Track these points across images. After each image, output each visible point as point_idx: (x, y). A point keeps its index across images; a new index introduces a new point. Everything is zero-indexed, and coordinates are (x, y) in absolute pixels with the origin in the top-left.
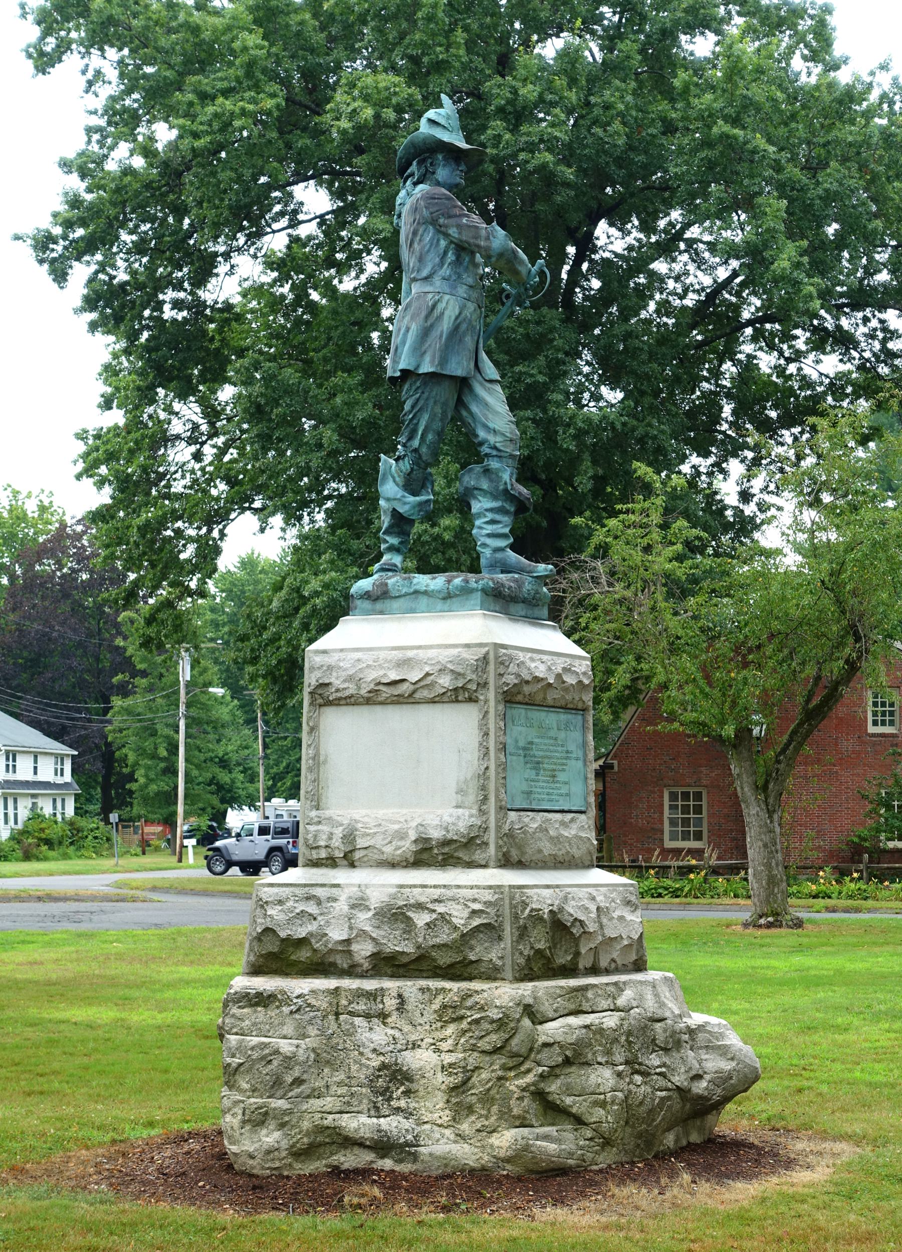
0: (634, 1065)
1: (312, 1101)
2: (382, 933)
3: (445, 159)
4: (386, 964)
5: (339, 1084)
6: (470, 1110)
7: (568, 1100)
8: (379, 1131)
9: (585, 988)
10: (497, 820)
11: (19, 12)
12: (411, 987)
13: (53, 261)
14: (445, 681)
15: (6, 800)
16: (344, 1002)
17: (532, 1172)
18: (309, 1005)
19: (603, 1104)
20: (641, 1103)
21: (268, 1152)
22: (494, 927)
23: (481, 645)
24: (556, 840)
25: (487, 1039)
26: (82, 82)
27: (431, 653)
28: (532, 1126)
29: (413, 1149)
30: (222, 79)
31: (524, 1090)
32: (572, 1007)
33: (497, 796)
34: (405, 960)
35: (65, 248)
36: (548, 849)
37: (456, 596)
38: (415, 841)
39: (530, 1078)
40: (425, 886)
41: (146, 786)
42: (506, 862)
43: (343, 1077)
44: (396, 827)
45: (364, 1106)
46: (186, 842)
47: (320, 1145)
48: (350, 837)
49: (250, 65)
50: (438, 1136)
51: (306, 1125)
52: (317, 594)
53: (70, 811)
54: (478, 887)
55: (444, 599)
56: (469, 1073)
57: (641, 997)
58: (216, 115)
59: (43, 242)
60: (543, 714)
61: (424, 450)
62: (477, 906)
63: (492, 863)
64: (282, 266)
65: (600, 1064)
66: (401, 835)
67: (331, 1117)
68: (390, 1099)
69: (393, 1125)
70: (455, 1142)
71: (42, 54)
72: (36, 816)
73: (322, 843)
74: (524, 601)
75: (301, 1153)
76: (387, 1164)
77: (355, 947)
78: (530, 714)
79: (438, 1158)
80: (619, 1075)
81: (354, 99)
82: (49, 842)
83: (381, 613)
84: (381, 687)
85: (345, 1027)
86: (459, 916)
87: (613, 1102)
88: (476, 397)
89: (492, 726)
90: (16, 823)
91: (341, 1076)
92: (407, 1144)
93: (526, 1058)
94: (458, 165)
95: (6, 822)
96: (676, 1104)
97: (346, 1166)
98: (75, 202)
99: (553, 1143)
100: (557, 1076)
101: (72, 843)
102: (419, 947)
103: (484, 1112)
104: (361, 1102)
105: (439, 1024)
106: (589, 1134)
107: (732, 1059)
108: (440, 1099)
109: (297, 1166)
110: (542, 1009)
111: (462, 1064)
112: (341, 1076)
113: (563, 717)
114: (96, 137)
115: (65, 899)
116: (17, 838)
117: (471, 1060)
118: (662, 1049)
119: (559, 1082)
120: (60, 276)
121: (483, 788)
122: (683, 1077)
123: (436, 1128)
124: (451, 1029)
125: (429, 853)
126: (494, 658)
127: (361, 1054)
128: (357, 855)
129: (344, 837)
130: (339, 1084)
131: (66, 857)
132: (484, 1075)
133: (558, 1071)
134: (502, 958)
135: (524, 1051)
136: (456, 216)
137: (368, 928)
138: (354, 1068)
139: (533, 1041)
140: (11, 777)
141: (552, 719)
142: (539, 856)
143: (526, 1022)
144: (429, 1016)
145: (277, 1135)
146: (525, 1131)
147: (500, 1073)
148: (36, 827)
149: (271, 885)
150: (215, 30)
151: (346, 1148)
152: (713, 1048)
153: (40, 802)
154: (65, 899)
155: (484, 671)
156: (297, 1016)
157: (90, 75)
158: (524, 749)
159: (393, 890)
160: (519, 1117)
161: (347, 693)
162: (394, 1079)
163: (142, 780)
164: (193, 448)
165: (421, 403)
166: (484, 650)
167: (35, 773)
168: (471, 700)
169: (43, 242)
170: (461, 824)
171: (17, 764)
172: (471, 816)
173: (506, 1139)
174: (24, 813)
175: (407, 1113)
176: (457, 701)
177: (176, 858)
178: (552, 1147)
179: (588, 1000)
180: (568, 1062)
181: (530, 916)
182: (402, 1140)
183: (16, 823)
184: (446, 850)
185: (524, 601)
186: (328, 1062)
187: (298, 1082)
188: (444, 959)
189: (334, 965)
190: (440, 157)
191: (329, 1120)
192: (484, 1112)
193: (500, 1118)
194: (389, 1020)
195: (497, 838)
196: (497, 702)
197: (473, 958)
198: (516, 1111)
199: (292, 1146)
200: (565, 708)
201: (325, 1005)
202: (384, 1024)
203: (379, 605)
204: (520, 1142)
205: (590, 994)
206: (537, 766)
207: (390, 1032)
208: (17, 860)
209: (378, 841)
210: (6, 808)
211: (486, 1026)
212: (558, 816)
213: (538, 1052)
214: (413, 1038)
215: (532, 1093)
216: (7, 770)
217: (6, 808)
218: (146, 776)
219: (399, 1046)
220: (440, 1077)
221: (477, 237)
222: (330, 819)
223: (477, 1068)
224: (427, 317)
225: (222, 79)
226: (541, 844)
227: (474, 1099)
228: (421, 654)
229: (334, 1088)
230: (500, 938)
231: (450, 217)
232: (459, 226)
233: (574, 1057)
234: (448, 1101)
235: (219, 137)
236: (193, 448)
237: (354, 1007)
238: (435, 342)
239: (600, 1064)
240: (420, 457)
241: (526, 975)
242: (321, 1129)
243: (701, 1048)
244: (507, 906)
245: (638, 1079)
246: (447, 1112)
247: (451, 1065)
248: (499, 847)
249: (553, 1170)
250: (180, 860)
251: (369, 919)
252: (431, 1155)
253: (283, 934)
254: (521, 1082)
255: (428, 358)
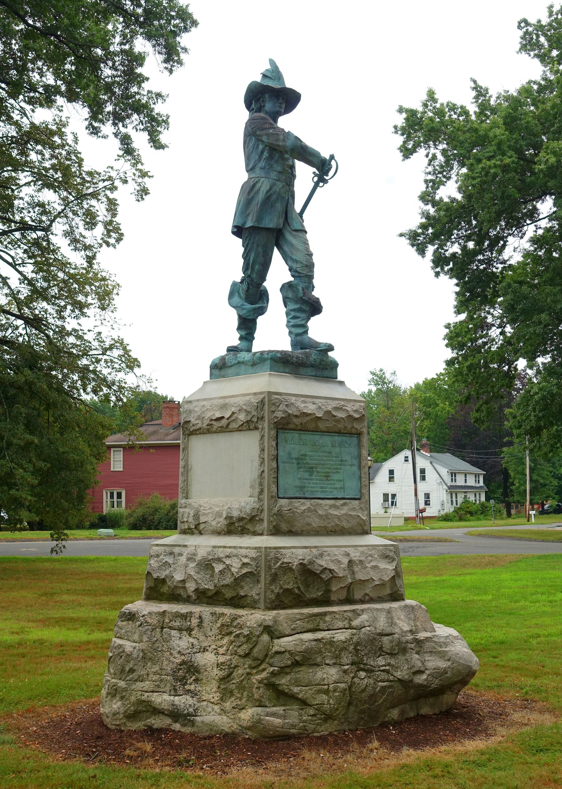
0: (358, 665)
1: (138, 683)
2: (200, 576)
3: (270, 97)
4: (203, 597)
5: (155, 673)
6: (231, 693)
7: (296, 690)
8: (173, 705)
9: (325, 614)
10: (269, 505)
11: (393, 130)
12: (205, 610)
13: (418, 245)
14: (242, 417)
15: (451, 494)
16: (167, 620)
17: (264, 737)
18: (146, 622)
19: (327, 692)
20: (363, 691)
21: (114, 714)
22: (254, 574)
23: (261, 393)
24: (327, 517)
25: (242, 648)
26: (426, 161)
27: (237, 400)
28: (266, 707)
29: (192, 718)
30: (488, 152)
31: (260, 682)
32: (310, 626)
33: (269, 490)
34: (210, 594)
35: (424, 238)
36: (316, 522)
37: (258, 363)
38: (226, 518)
39: (264, 675)
40: (225, 547)
41: (519, 487)
42: (276, 531)
43: (157, 668)
44: (217, 509)
45: (168, 689)
46: (531, 512)
47: (141, 712)
48: (197, 516)
49: (499, 144)
50: (210, 710)
51: (133, 699)
52: (537, 393)
53: (483, 499)
54: (250, 548)
55: (252, 366)
56: (233, 668)
57: (375, 619)
58: (483, 168)
59: (413, 237)
60: (319, 437)
61: (254, 275)
62: (246, 560)
63: (265, 533)
64: (534, 241)
65: (328, 665)
66: (219, 514)
67: (146, 694)
68: (186, 684)
69: (183, 701)
70: (220, 714)
71: (407, 149)
72: (466, 501)
73: (185, 520)
74: (312, 366)
75: (132, 716)
76: (177, 727)
77: (187, 585)
78: (303, 437)
79: (207, 724)
80: (345, 672)
81: (548, 154)
82: (471, 513)
83: (224, 377)
84: (213, 422)
85: (165, 636)
86: (235, 565)
87: (335, 691)
88: (286, 241)
89: (266, 445)
90: (457, 504)
91: (156, 668)
92: (189, 714)
93: (263, 661)
94: (278, 100)
95: (452, 504)
96: (399, 690)
97: (155, 726)
98: (427, 216)
99: (277, 718)
100: (287, 674)
101: (481, 514)
102: (215, 586)
103: (239, 695)
104: (166, 685)
105: (220, 636)
106: (312, 712)
107: (449, 660)
108: (214, 685)
109: (129, 724)
110: (281, 628)
111: (228, 663)
112: (156, 668)
113: (337, 439)
114: (431, 184)
115: (413, 541)
116: (456, 511)
117: (234, 662)
118: (388, 654)
119: (289, 677)
120: (422, 251)
121: (261, 484)
122: (405, 673)
123: (210, 704)
124: (226, 640)
125: (236, 526)
126: (268, 401)
127: (171, 654)
128: (202, 527)
129: (194, 516)
130: (155, 673)
131: (478, 519)
132: (240, 671)
133: (288, 670)
134: (258, 594)
135: (261, 656)
136: (266, 129)
137: (192, 573)
138: (165, 663)
139: (268, 650)
140: (454, 484)
141: (327, 440)
142: (309, 528)
143: (265, 638)
144: (215, 631)
145: (119, 703)
146: (260, 709)
147: (248, 670)
148: (465, 506)
149: (157, 545)
150: (485, 130)
151: (155, 715)
152: (435, 652)
153: (468, 495)
154: (413, 541)
155: (262, 409)
156: (140, 629)
157: (430, 156)
158: (297, 459)
159: (210, 549)
160: (257, 700)
161: (198, 427)
162: (189, 671)
163: (517, 485)
164: (500, 330)
165: (250, 246)
166: (262, 396)
167: (466, 482)
168: (256, 428)
169: (413, 237)
170: (248, 507)
171: (457, 478)
172: (254, 502)
173: (248, 715)
174: (460, 499)
175: (193, 694)
176: (250, 429)
177: (527, 519)
178: (277, 721)
179: (325, 622)
180: (296, 664)
181: (280, 567)
182: (186, 712)
183: (457, 504)
184: (241, 524)
185: (312, 366)
186: (150, 659)
187: (132, 671)
188: (229, 594)
189: (180, 595)
190: (267, 96)
191: (145, 696)
192: (239, 695)
193: (248, 700)
194: (193, 633)
195: (269, 516)
196: (270, 429)
197: (243, 594)
198: (256, 696)
199: (126, 712)
200: (339, 433)
201: (155, 622)
202: (190, 635)
203: (223, 372)
204: (256, 717)
205: (328, 618)
206: (311, 470)
207: (191, 640)
208: (456, 521)
209: (209, 518)
210: (452, 498)
211: (242, 639)
212: (332, 502)
213: (271, 658)
214: (205, 644)
215: (265, 685)
216: (452, 481)
217: (452, 498)
218: (519, 483)
219: (195, 650)
220: (216, 671)
221: (277, 140)
222: (190, 504)
223: (236, 666)
224: (249, 193)
225: (488, 152)
226: (310, 520)
227: (234, 686)
228: (232, 400)
229: (151, 675)
230: (258, 582)
231: (263, 129)
232: (267, 135)
233: (304, 660)
234: (219, 687)
235: (484, 178)
236: (500, 330)
237: (173, 624)
238: (255, 207)
239: (328, 665)
240: (252, 280)
241: (277, 604)
242: (141, 702)
243: (427, 652)
244: (263, 561)
245: (362, 674)
246: (218, 694)
247: (222, 664)
248: (270, 522)
249: (279, 736)
250: (528, 521)
251: (194, 568)
252: (202, 722)
253: (155, 576)
254: (259, 677)
255: (250, 218)
